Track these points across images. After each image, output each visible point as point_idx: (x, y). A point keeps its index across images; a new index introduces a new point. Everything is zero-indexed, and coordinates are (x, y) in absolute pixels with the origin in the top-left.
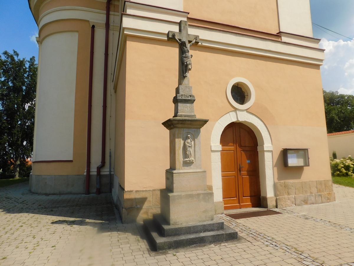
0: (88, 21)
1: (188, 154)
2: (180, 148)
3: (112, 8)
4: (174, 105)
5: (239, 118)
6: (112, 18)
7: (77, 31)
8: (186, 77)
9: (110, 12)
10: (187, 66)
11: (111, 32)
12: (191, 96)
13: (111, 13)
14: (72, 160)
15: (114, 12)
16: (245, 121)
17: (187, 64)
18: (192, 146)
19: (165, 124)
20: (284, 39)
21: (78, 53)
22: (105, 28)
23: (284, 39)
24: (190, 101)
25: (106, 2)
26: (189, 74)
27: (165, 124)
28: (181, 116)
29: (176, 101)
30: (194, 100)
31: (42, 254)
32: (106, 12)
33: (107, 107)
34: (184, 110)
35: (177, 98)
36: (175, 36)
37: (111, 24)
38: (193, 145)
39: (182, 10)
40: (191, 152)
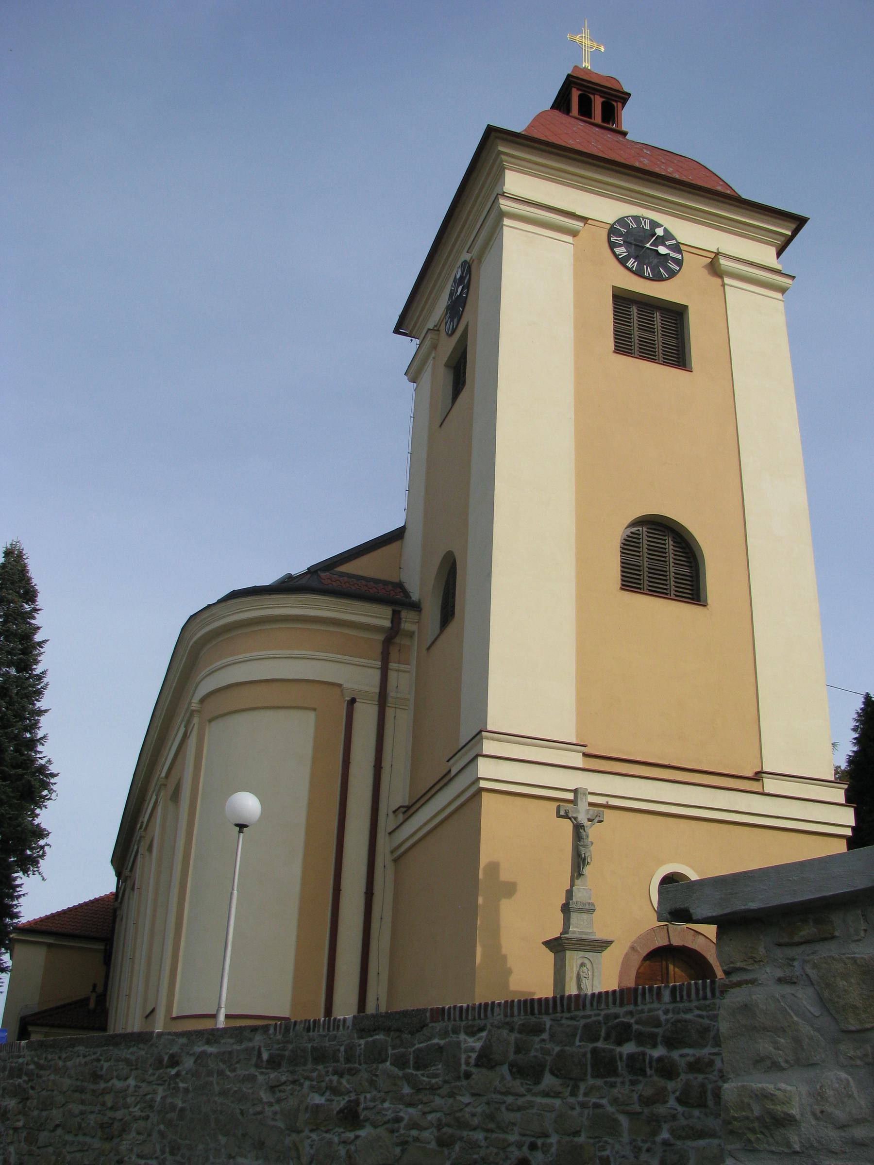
0: (340, 685)
1: (583, 988)
2: (571, 978)
3: (394, 654)
4: (563, 915)
5: (671, 938)
6: (392, 676)
7: (315, 709)
8: (583, 875)
9: (390, 664)
10: (585, 859)
11: (390, 713)
12: (589, 904)
13: (392, 665)
14: (288, 1018)
15: (399, 663)
16: (683, 945)
17: (585, 856)
18: (588, 977)
19: (548, 944)
20: (770, 785)
21: (315, 760)
22: (377, 703)
23: (770, 785)
24: (589, 909)
25: (383, 639)
26: (587, 870)
27: (548, 944)
28: (574, 932)
29: (566, 909)
30: (594, 910)
31: (838, 747)
32: (380, 663)
33: (375, 894)
34: (579, 926)
35: (570, 907)
36: (569, 812)
37: (392, 693)
38: (591, 977)
39: (574, 741)
40: (588, 986)
